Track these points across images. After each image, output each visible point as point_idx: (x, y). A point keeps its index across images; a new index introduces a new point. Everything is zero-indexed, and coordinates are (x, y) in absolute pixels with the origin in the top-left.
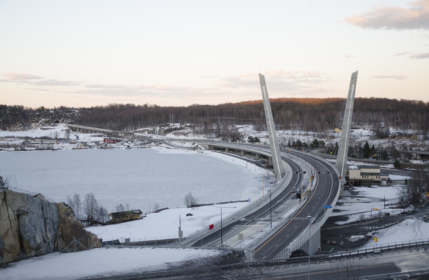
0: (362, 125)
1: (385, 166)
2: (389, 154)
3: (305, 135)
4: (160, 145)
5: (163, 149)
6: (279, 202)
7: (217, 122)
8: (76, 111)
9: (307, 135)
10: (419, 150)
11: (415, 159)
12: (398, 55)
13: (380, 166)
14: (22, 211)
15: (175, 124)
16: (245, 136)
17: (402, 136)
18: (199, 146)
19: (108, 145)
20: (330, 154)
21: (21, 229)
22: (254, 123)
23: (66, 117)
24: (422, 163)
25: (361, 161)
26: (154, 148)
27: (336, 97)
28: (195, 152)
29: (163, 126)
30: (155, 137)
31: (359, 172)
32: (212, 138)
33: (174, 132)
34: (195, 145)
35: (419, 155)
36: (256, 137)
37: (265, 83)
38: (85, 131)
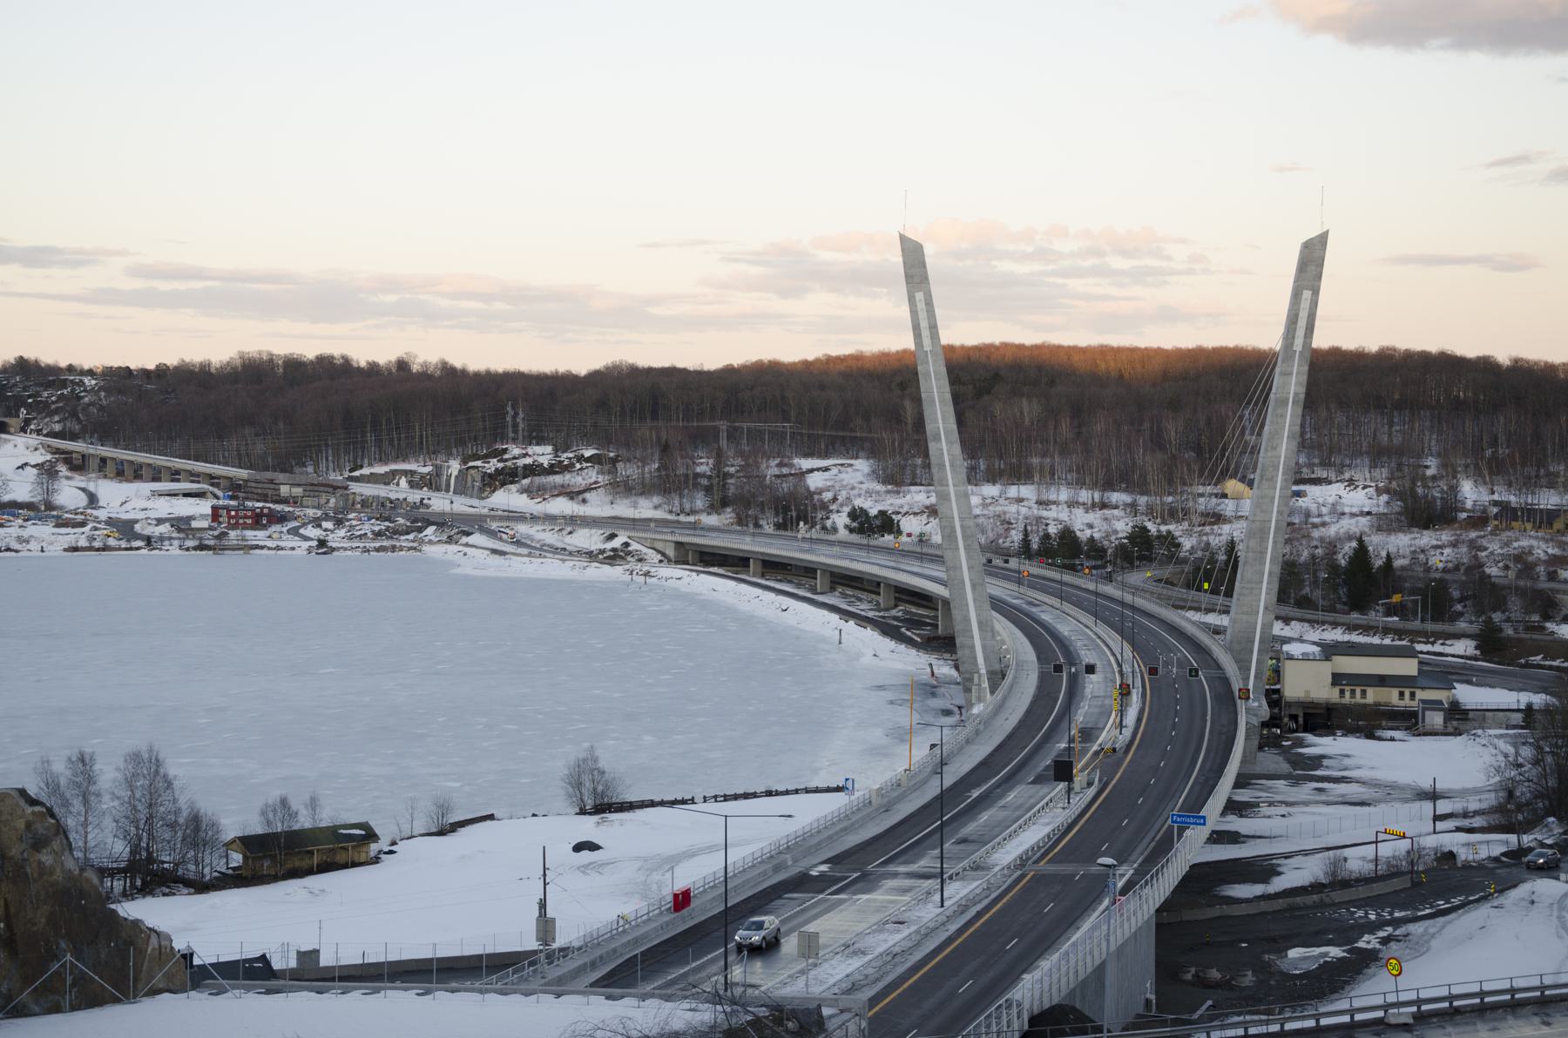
1: (1437, 648)
2: (1456, 594)
3: (1094, 505)
4: (465, 539)
5: (473, 559)
6: (976, 794)
7: (713, 446)
8: (87, 380)
9: (1104, 506)
13: (1419, 647)
15: (530, 450)
18: (634, 546)
19: (232, 534)
20: (1200, 589)
23: (43, 409)
25: (1335, 625)
26: (437, 551)
27: (1231, 345)
28: (616, 572)
29: (476, 457)
30: (439, 503)
31: (1326, 669)
32: (693, 512)
33: (526, 482)
34: (617, 543)
36: (882, 513)
38: (128, 471)
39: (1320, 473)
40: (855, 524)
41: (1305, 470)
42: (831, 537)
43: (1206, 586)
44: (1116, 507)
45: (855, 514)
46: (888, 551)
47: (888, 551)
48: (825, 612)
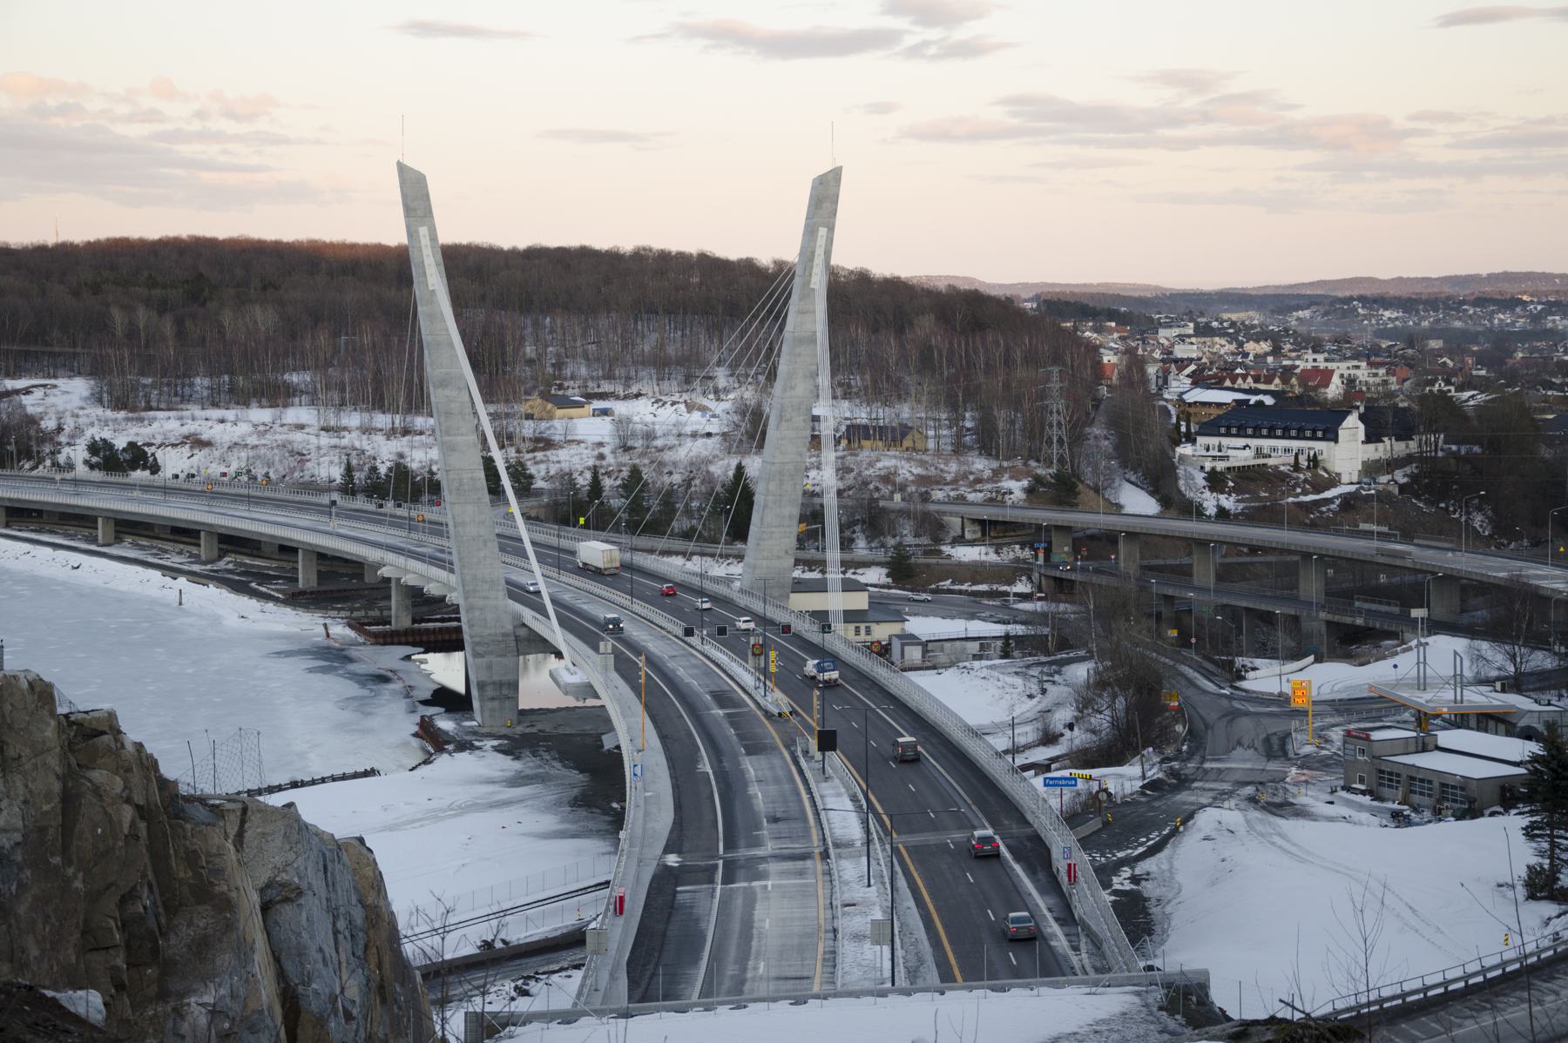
0: (628, 378)
6: (706, 766)
9: (406, 432)
10: (961, 499)
11: (960, 540)
12: (692, 32)
14: (283, 885)
16: (63, 439)
17: (867, 437)
21: (289, 967)
22: (95, 370)
24: (993, 557)
27: (465, 242)
35: (974, 521)
36: (132, 445)
37: (428, 212)
39: (606, 387)
40: (95, 460)
41: (590, 384)
42: (69, 476)
43: (582, 521)
44: (421, 433)
45: (93, 448)
46: (146, 488)
47: (146, 488)
48: (139, 569)
